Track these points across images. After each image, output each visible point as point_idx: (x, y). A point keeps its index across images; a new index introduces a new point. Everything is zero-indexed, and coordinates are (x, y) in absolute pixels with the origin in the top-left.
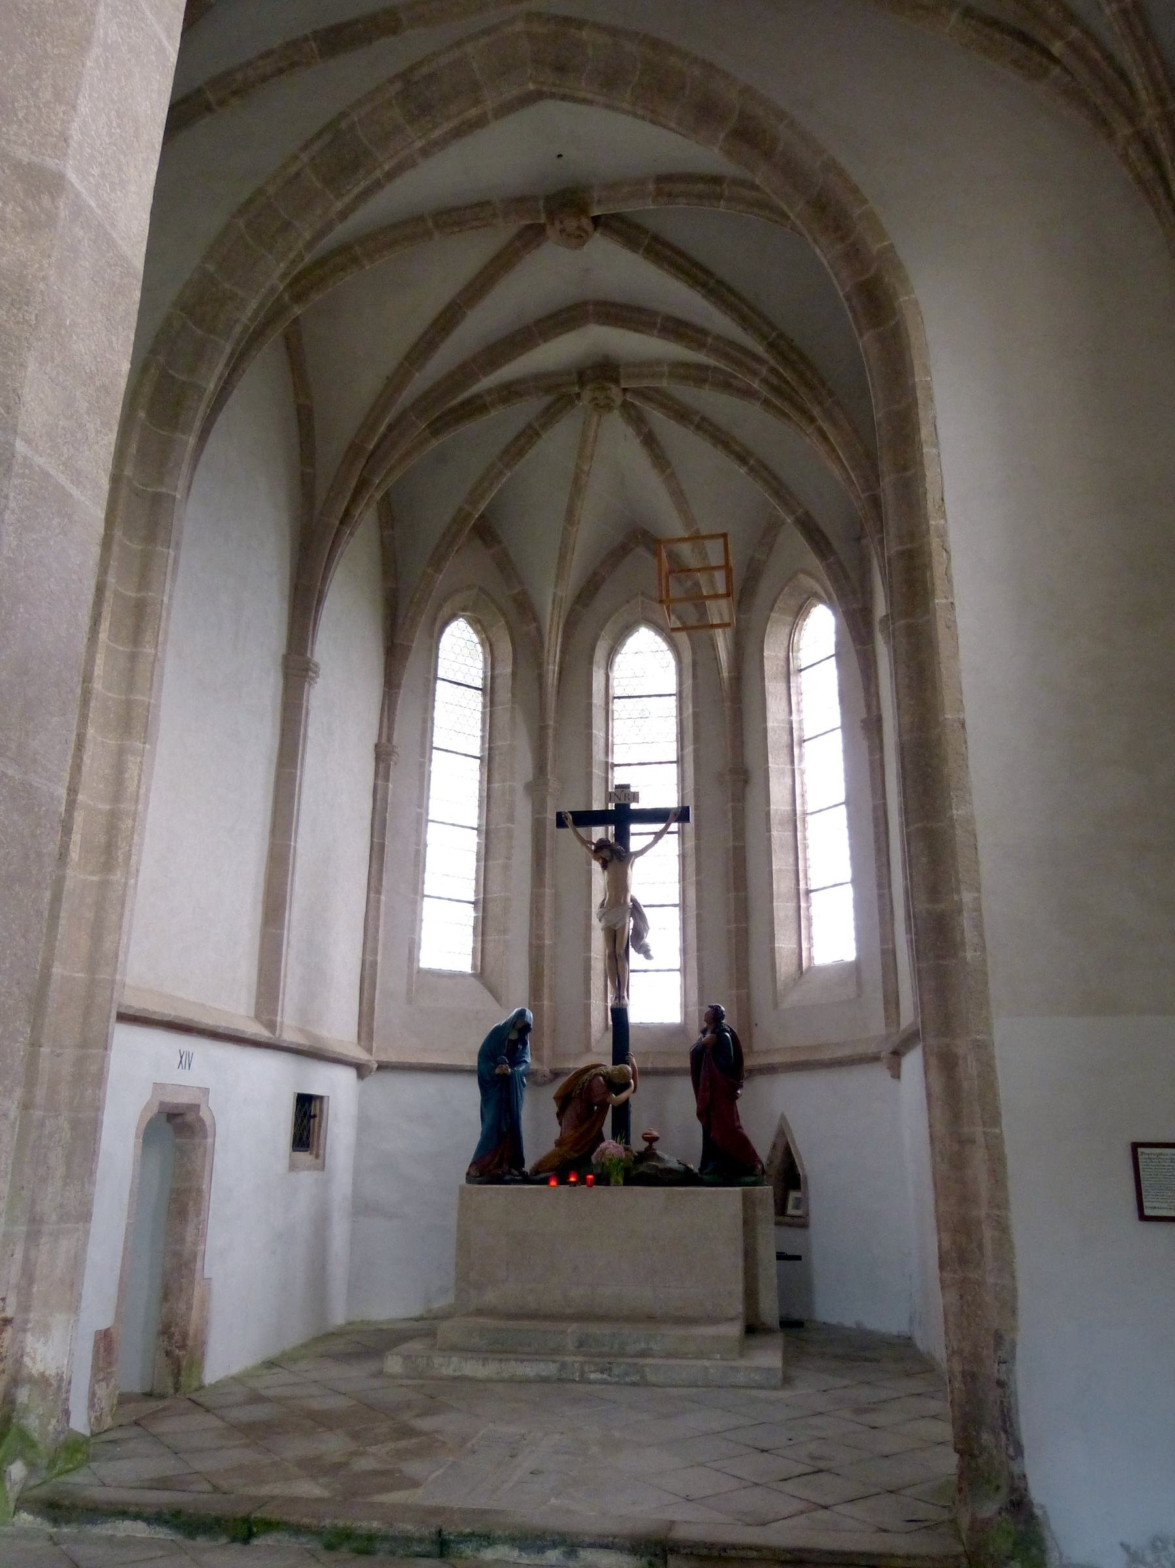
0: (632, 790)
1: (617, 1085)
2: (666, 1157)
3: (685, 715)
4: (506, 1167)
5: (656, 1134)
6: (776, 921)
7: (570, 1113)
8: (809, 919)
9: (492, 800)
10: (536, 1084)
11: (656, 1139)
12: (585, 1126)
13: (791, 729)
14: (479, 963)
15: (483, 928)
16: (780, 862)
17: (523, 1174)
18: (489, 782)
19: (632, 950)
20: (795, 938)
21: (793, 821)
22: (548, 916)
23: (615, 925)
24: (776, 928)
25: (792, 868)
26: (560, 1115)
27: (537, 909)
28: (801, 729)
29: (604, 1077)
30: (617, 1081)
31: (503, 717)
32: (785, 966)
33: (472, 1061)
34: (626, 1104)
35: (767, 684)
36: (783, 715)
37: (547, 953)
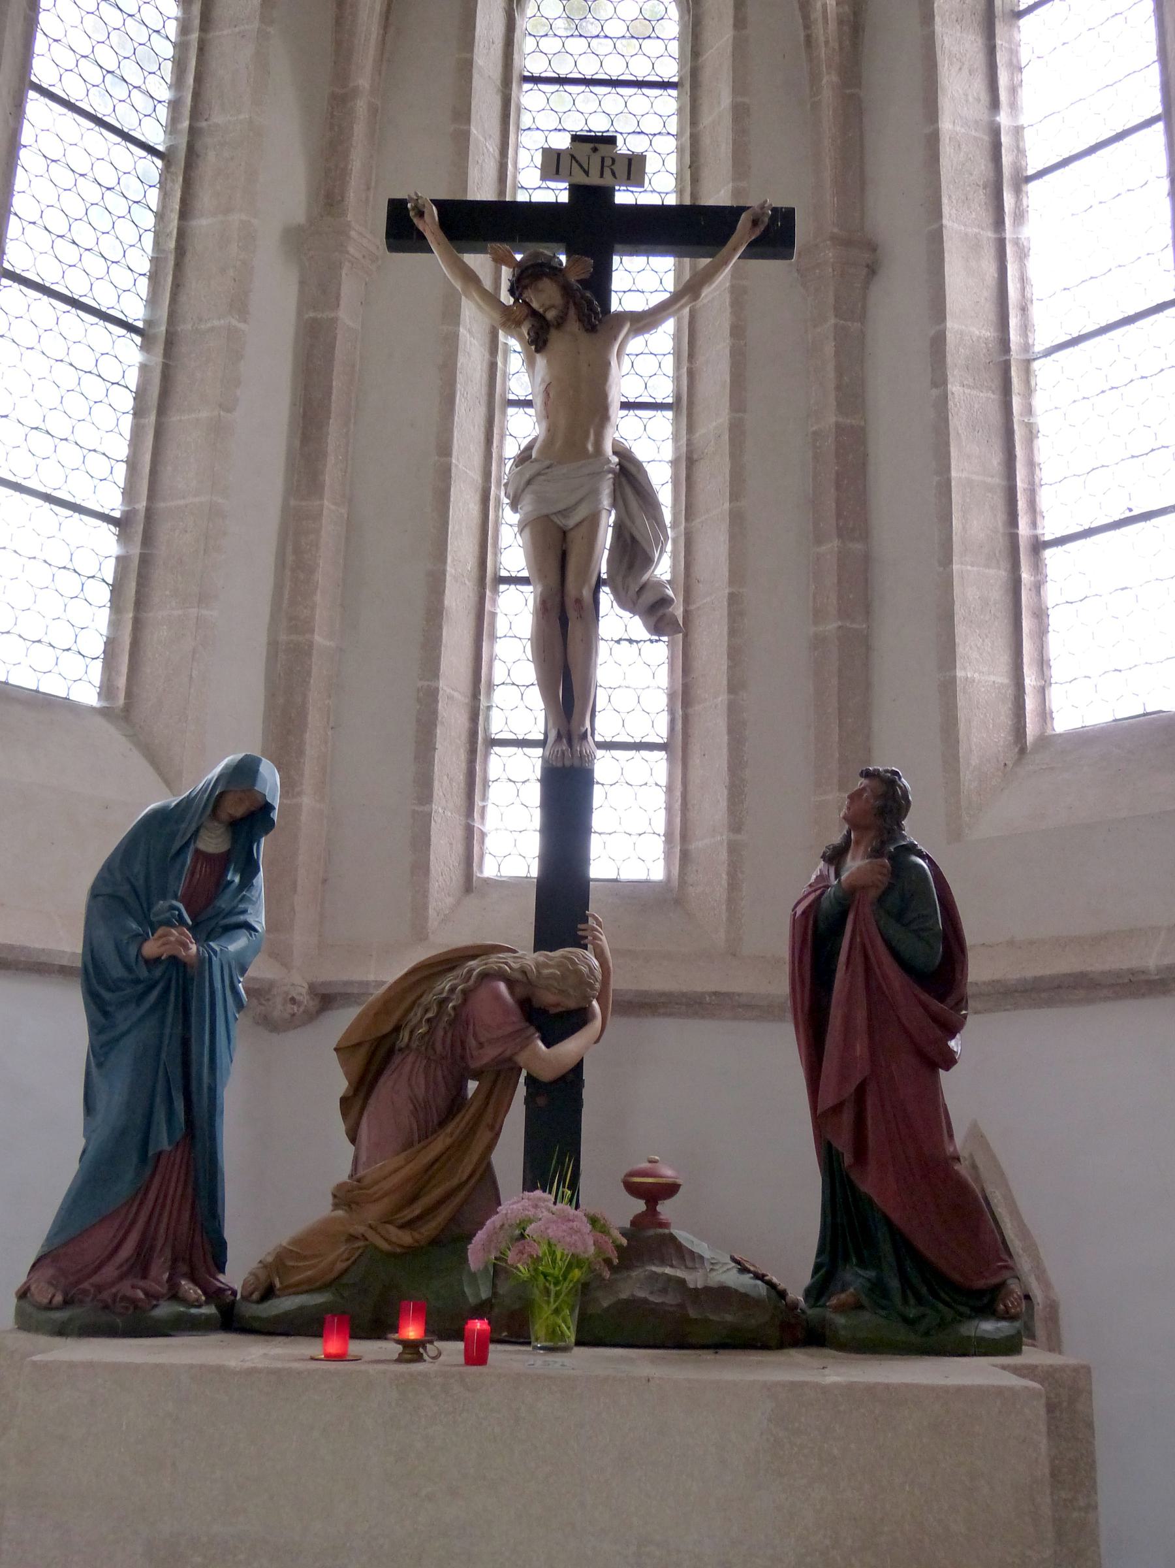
0: (622, 148)
1: (553, 1017)
2: (701, 1247)
3: (706, 120)
4: (160, 1272)
5: (668, 1173)
6: (959, 612)
7: (398, 1089)
8: (1041, 615)
9: (190, 262)
10: (268, 1023)
11: (671, 1189)
12: (439, 1144)
13: (996, 147)
14: (122, 682)
15: (136, 590)
16: (970, 462)
17: (215, 1295)
18: (184, 215)
19: (606, 597)
20: (1004, 659)
21: (1004, 372)
22: (326, 571)
23: (565, 512)
24: (960, 629)
25: (998, 481)
26: (354, 1104)
27: (297, 551)
28: (1020, 151)
29: (511, 983)
30: (547, 998)
31: (234, 53)
32: (982, 732)
33: (68, 941)
34: (573, 1078)
35: (939, 27)
36: (977, 111)
37: (319, 669)
